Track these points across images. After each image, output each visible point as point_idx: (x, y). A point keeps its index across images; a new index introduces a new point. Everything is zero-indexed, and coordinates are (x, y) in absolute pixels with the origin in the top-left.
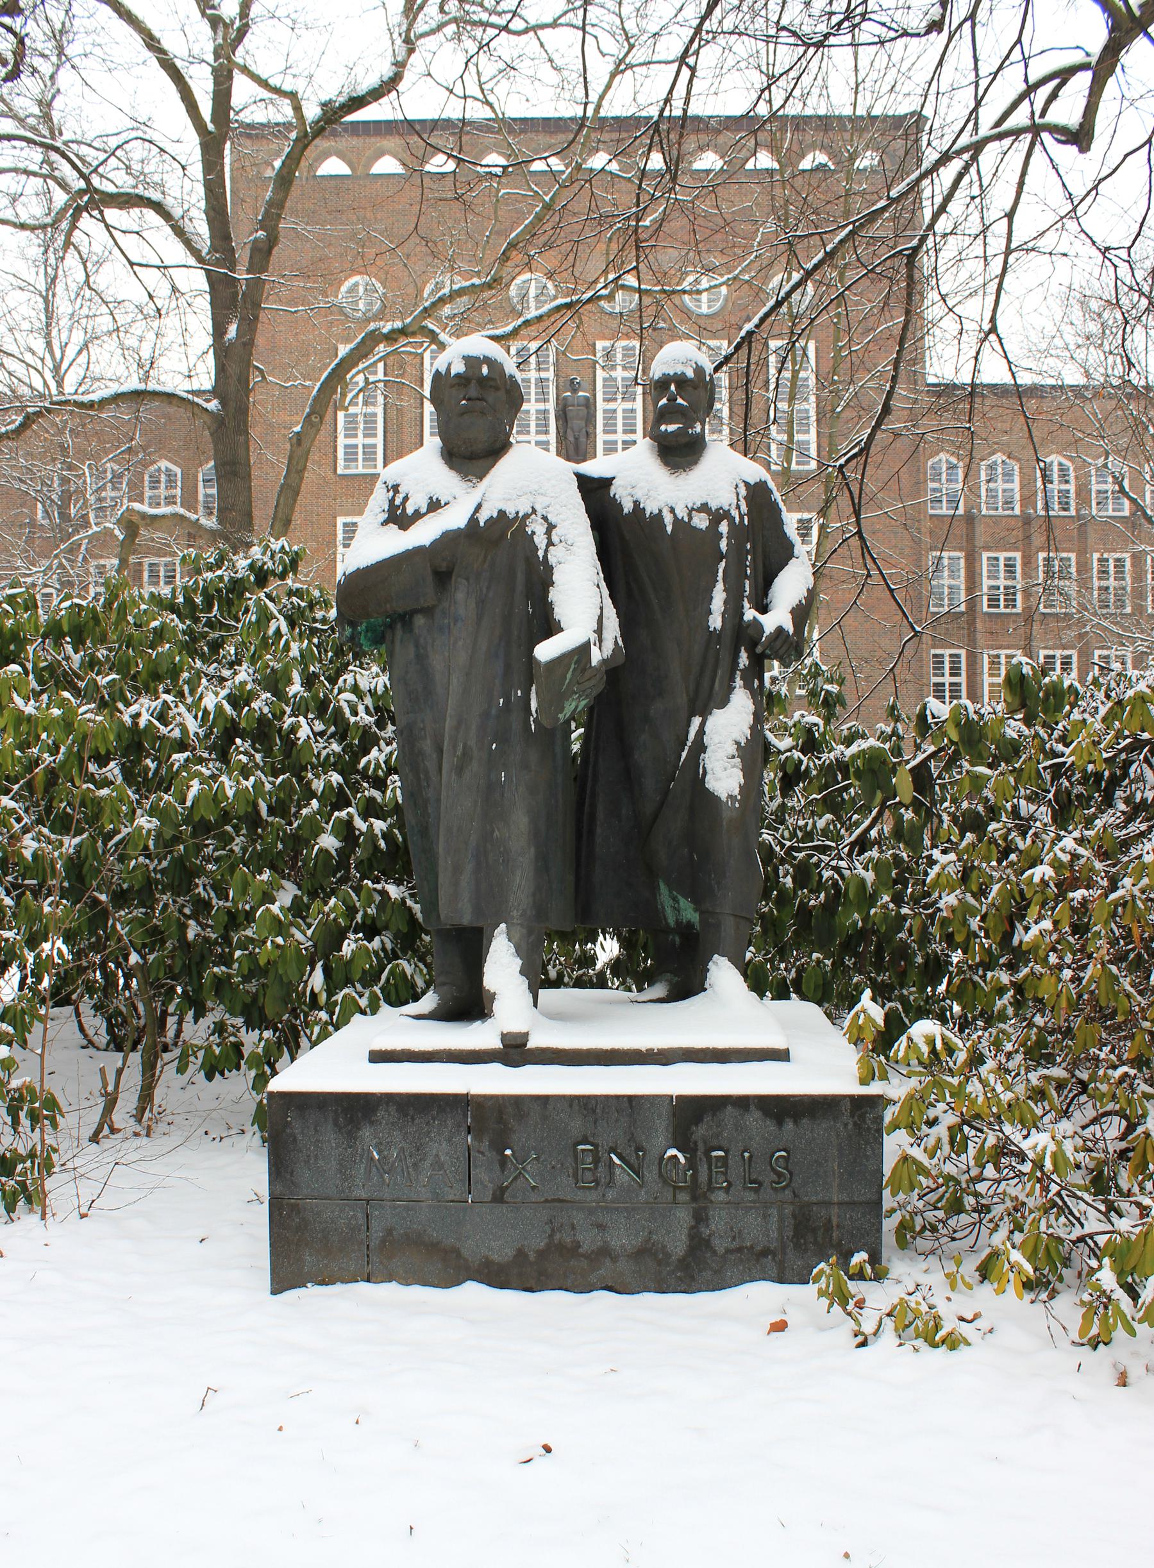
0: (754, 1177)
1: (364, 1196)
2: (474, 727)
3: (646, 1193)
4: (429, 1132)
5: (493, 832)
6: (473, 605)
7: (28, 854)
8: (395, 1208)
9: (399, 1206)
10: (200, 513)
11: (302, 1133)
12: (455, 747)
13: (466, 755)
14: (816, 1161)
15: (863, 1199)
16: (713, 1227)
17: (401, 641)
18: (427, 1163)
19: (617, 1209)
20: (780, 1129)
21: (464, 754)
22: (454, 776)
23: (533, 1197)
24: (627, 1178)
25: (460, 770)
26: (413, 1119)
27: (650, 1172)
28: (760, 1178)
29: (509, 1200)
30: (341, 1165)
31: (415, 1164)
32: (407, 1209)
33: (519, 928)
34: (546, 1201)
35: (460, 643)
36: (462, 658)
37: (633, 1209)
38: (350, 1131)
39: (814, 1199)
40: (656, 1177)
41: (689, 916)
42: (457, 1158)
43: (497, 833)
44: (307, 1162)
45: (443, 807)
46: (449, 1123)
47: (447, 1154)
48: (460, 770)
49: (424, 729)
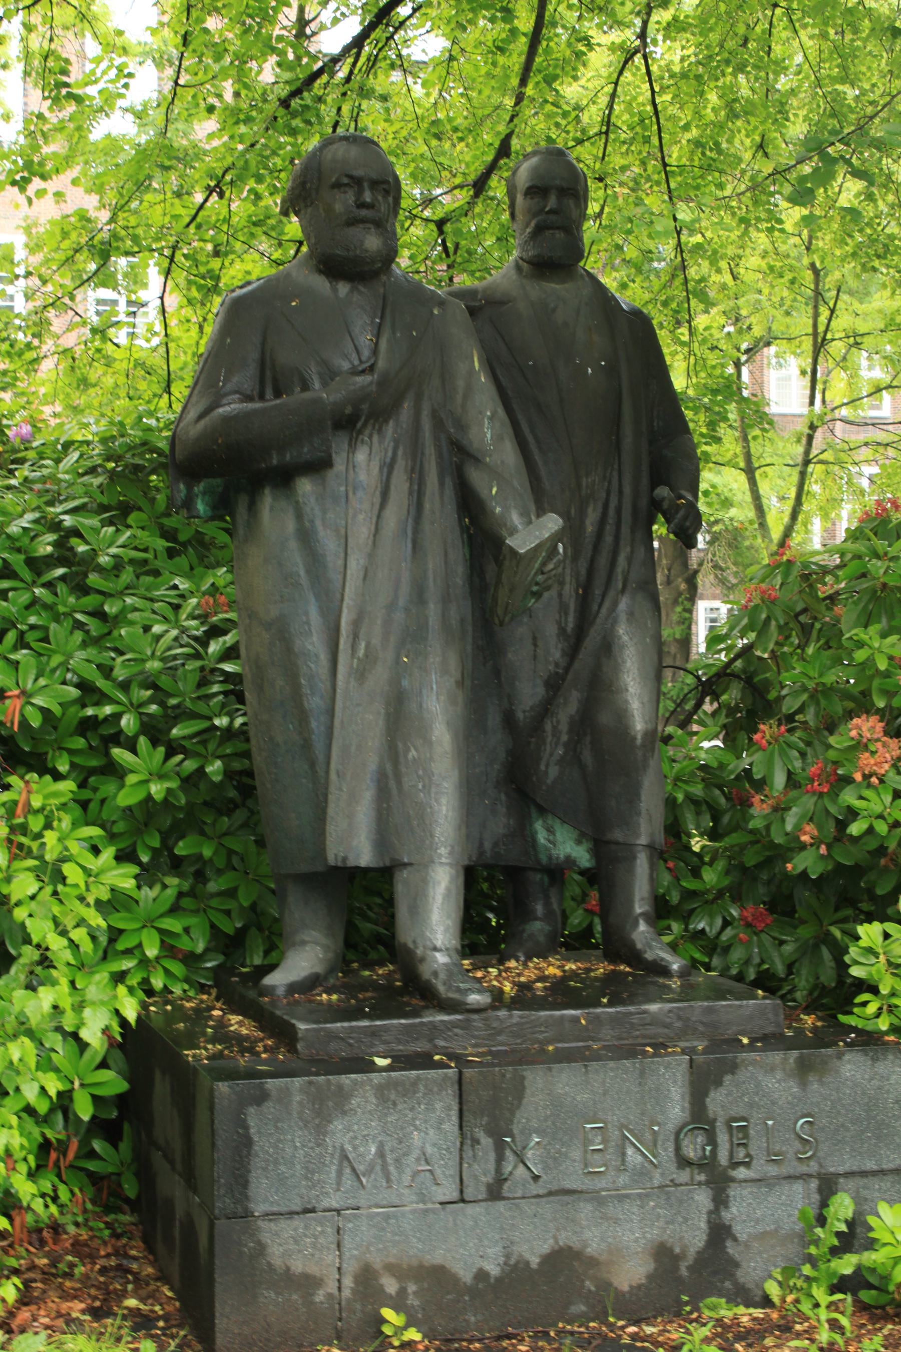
0: (777, 1148)
1: (335, 1205)
2: (379, 622)
3: (662, 1174)
4: (414, 1119)
5: (408, 750)
6: (376, 471)
7: (552, 523)
8: (371, 1217)
9: (378, 1214)
10: (119, 229)
11: (259, 1132)
12: (354, 647)
13: (370, 658)
14: (843, 1125)
15: (891, 1166)
16: (734, 1210)
17: (272, 509)
18: (412, 1158)
19: (627, 1196)
20: (804, 1090)
21: (366, 656)
22: (353, 683)
23: (535, 1189)
24: (640, 1159)
25: (360, 674)
26: (395, 1104)
27: (665, 1150)
28: (784, 1149)
29: (511, 1195)
30: (307, 1168)
31: (397, 1160)
32: (387, 1217)
33: (447, 868)
34: (550, 1194)
35: (361, 517)
36: (362, 532)
37: (647, 1195)
38: (318, 1126)
39: (841, 1170)
40: (672, 1155)
41: (568, 850)
42: (447, 1150)
43: (413, 753)
44: (265, 1169)
45: (337, 722)
46: (438, 1105)
47: (434, 1145)
48: (360, 674)
49: (308, 623)
